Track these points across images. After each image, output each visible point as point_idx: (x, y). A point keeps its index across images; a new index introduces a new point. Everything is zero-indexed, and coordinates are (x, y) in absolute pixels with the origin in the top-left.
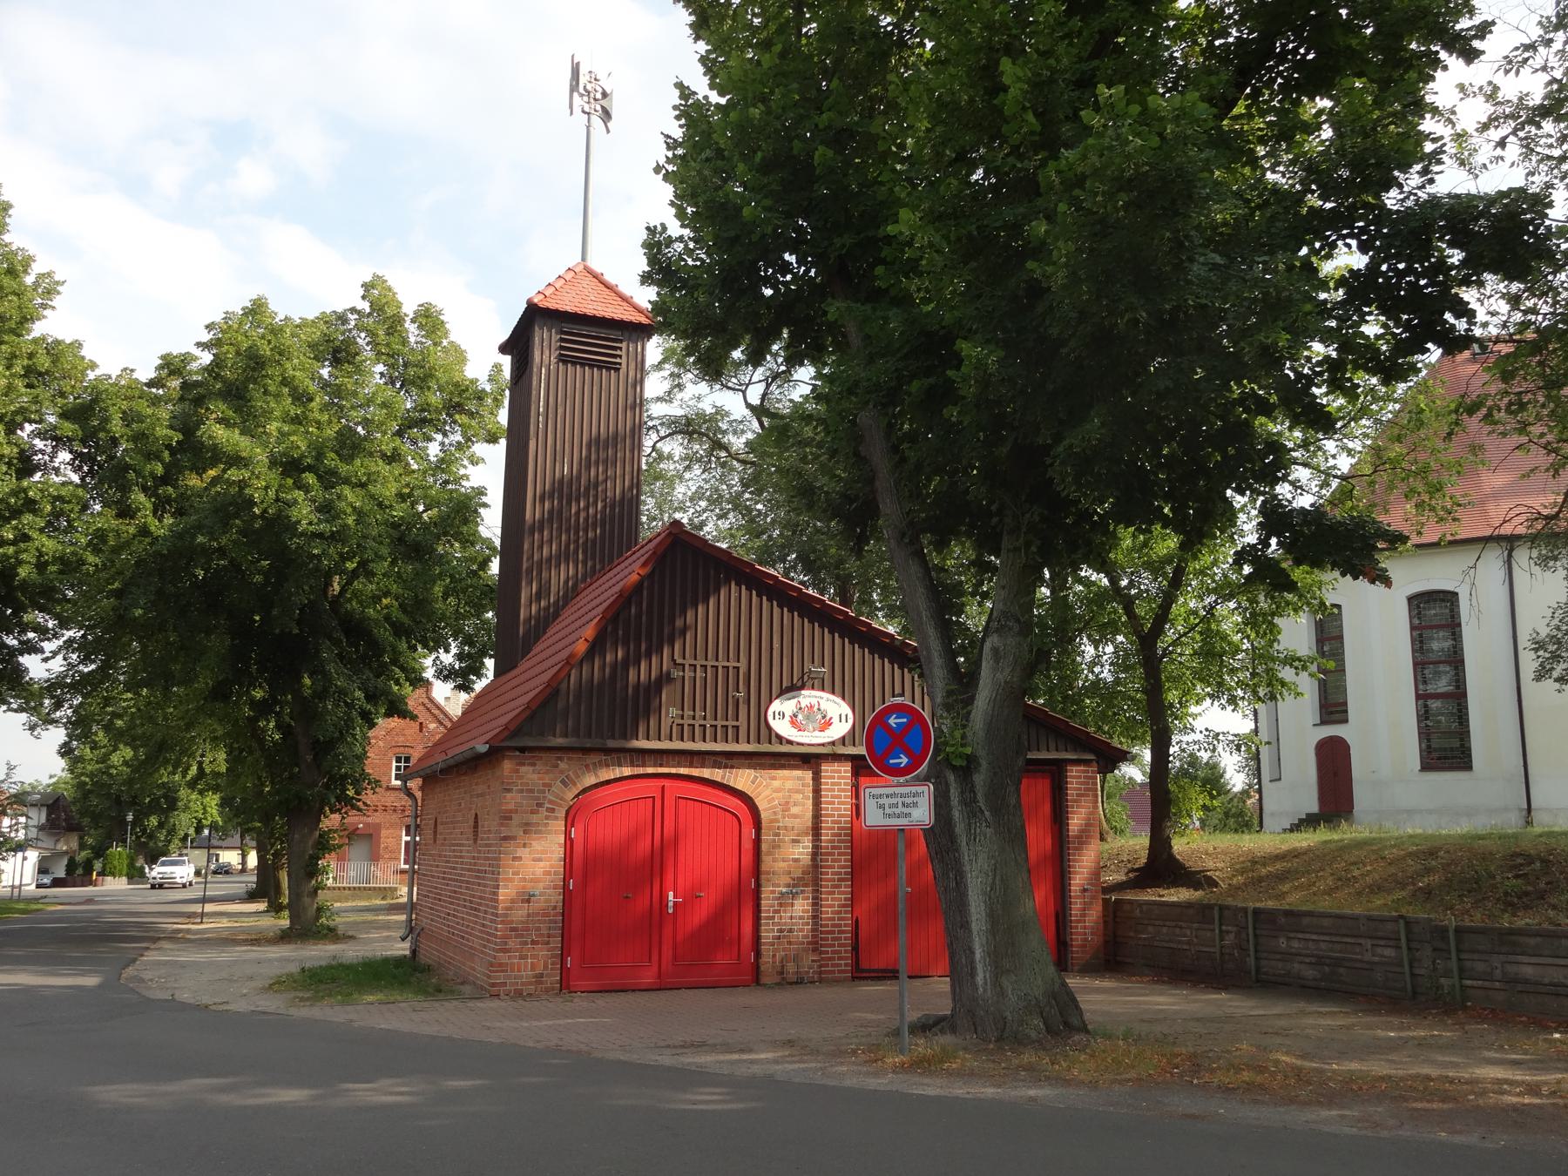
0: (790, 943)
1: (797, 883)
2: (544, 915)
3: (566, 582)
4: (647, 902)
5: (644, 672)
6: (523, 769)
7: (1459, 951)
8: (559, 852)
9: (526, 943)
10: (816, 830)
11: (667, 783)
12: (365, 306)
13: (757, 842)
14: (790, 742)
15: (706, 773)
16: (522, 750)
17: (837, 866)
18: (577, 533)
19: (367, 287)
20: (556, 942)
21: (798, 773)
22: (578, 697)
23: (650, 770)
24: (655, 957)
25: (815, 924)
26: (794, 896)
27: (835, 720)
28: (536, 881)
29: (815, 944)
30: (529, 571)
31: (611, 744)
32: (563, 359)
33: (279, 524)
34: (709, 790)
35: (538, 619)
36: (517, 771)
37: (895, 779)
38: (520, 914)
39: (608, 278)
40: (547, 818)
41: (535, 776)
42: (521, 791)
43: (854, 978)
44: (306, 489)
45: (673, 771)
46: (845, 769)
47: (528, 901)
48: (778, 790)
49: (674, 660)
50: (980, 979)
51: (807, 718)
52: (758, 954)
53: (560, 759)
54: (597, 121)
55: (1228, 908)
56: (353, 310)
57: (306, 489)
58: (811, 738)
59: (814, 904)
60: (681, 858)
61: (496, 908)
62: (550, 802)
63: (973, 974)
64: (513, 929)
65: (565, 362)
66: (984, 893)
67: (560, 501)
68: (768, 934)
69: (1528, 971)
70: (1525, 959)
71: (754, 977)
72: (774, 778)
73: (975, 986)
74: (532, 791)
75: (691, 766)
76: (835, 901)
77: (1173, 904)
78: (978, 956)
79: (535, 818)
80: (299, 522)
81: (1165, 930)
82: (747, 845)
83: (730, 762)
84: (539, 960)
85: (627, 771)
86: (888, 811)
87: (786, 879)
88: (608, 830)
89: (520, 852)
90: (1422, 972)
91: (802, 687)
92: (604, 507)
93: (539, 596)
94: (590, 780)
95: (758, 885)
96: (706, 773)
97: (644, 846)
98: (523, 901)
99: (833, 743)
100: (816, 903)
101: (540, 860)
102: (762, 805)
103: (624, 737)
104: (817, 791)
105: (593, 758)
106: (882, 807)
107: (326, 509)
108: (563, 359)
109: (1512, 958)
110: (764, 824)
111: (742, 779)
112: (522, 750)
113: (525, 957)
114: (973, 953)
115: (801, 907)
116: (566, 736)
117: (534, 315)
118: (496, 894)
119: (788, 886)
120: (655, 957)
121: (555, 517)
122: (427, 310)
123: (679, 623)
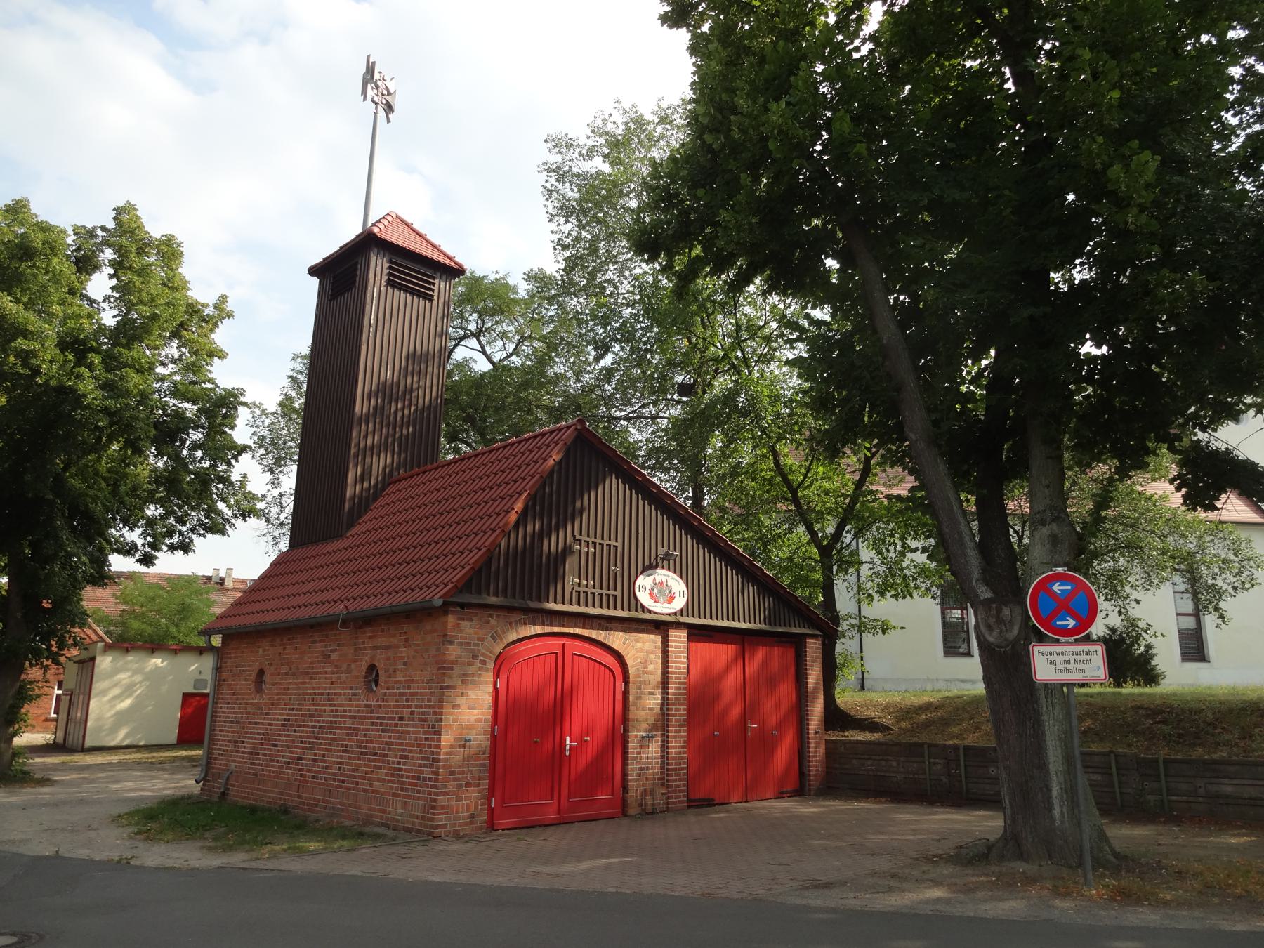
0: (647, 779)
1: (652, 728)
2: (477, 759)
3: (385, 468)
4: (550, 746)
5: (552, 544)
6: (464, 624)
7: (1166, 776)
8: (488, 701)
9: (461, 786)
10: (664, 684)
11: (569, 642)
12: (111, 225)
13: (626, 694)
14: (649, 611)
15: (593, 634)
16: (462, 606)
17: (678, 715)
18: (394, 429)
19: (119, 211)
20: (485, 784)
21: (652, 636)
22: (506, 560)
23: (556, 629)
24: (556, 796)
25: (663, 763)
26: (650, 738)
27: (677, 595)
28: (470, 727)
29: (664, 780)
30: (356, 455)
31: (534, 604)
32: (390, 283)
33: (66, 395)
34: (600, 651)
35: (361, 498)
36: (458, 625)
37: (1064, 639)
38: (458, 757)
39: (415, 226)
40: (480, 669)
41: (472, 631)
42: (461, 644)
43: (689, 807)
44: (90, 367)
45: (571, 631)
46: (683, 634)
47: (464, 746)
48: (640, 650)
49: (573, 536)
50: (1056, 812)
51: (660, 592)
52: (625, 788)
53: (491, 616)
54: (381, 113)
55: (936, 746)
56: (103, 228)
57: (90, 367)
58: (663, 609)
59: (662, 746)
60: (574, 707)
61: (439, 753)
62: (483, 655)
63: (1050, 808)
64: (452, 773)
65: (393, 287)
66: (1060, 739)
67: (383, 400)
68: (633, 772)
69: (1229, 789)
70: (1226, 781)
71: (621, 809)
72: (637, 641)
73: (1052, 820)
74: (469, 644)
75: (584, 627)
76: (677, 741)
77: (861, 742)
78: (1055, 791)
79: (471, 669)
80: (85, 396)
81: (870, 762)
82: (619, 696)
83: (609, 625)
84: (467, 802)
85: (539, 629)
86: (1059, 666)
87: (644, 726)
88: (527, 679)
89: (460, 701)
90: (1130, 790)
91: (656, 567)
92: (416, 410)
93: (362, 479)
94: (513, 636)
95: (626, 731)
96: (593, 634)
97: (549, 695)
98: (460, 746)
99: (675, 614)
100: (665, 746)
101: (474, 708)
102: (630, 663)
103: (539, 600)
104: (665, 652)
105: (515, 617)
106: (1053, 663)
107: (109, 387)
108: (390, 283)
109: (1214, 780)
110: (631, 678)
111: (617, 639)
112: (462, 606)
113: (459, 799)
114: (1049, 790)
115: (654, 748)
116: (496, 595)
117: (367, 242)
118: (439, 740)
119: (646, 731)
120: (556, 796)
121: (378, 412)
122: (169, 240)
123: (578, 504)
